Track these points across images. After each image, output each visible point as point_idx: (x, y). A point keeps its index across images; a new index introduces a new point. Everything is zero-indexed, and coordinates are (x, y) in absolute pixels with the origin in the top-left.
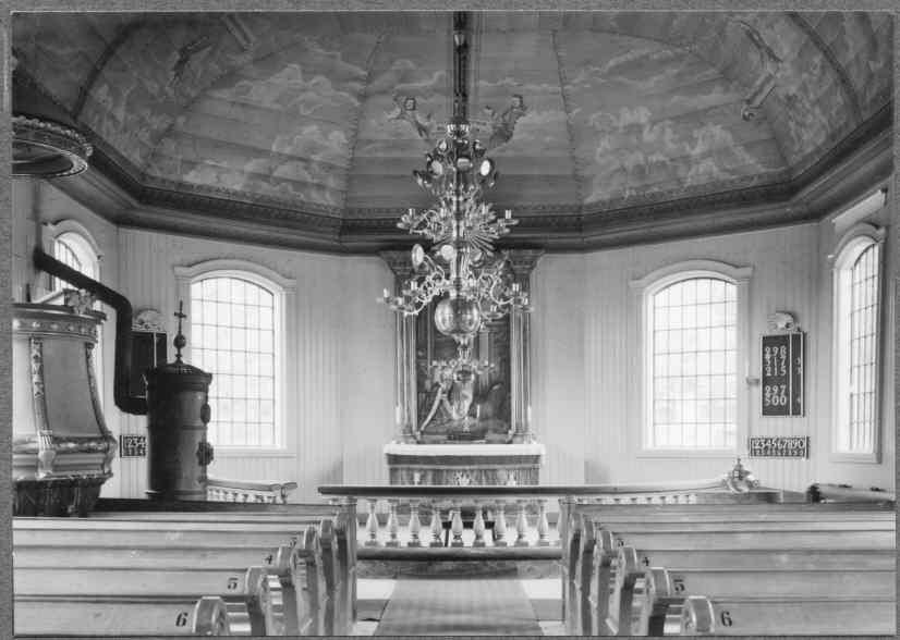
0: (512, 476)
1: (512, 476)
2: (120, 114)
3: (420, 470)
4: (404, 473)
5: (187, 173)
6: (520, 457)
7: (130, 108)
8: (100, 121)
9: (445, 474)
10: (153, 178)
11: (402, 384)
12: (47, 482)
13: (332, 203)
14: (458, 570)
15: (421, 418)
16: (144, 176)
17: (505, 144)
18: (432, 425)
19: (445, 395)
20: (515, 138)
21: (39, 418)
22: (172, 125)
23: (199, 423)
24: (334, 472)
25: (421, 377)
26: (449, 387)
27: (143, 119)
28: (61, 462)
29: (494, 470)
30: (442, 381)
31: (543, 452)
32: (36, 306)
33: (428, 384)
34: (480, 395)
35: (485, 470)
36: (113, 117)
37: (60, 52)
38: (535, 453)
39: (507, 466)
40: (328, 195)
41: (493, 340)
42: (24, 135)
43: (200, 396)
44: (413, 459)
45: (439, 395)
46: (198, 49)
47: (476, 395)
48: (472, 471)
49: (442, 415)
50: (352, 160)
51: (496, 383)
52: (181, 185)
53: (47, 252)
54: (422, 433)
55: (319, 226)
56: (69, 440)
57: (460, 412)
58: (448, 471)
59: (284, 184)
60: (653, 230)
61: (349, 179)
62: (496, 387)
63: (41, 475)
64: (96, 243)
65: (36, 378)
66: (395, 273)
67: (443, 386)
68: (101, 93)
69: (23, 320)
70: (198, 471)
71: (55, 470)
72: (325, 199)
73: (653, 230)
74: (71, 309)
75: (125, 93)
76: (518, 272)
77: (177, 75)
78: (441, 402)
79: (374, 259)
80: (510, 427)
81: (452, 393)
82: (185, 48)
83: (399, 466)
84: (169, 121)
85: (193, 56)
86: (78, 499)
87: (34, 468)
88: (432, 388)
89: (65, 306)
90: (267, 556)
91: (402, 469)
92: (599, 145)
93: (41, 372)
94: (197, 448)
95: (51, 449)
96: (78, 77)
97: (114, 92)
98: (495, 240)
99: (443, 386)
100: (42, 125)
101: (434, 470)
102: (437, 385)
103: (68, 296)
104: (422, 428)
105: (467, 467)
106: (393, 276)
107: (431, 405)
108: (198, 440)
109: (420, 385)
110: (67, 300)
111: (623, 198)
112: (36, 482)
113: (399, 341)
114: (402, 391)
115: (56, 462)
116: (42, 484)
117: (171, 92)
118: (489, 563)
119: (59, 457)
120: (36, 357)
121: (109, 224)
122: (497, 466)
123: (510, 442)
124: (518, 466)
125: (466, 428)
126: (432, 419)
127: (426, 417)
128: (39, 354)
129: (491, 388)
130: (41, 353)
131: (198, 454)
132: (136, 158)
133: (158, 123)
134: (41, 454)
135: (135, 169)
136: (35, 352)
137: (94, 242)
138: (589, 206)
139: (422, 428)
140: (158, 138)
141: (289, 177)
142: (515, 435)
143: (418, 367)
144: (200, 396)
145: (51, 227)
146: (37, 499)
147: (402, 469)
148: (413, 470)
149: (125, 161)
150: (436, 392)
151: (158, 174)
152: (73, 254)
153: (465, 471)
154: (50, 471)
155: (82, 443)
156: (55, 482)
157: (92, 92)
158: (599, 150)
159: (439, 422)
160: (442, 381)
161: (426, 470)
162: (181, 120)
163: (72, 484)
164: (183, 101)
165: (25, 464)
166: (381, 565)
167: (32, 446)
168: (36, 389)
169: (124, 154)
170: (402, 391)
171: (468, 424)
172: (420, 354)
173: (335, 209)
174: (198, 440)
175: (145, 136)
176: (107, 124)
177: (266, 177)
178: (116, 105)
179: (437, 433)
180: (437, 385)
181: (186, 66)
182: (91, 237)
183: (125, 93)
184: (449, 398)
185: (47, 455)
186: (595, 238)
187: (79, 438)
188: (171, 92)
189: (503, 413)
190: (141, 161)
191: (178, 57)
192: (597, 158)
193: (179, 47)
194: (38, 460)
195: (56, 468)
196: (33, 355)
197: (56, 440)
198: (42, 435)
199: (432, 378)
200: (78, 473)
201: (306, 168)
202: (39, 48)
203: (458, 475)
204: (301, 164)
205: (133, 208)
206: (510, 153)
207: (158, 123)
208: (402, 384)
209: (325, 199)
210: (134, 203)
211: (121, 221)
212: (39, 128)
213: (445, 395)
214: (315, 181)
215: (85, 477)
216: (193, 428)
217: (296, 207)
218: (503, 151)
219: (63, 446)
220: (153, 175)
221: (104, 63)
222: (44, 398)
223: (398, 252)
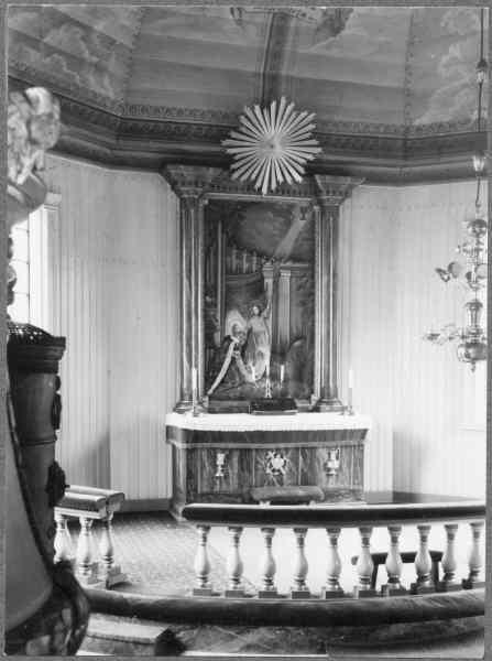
0: (333, 456)
1: (333, 456)
3: (223, 450)
4: (205, 453)
6: (334, 433)
9: (254, 453)
11: (189, 339)
13: (111, 95)
14: (407, 636)
15: (208, 379)
17: (332, 39)
18: (221, 389)
19: (238, 352)
20: (345, 32)
24: (101, 448)
25: (209, 330)
26: (243, 343)
29: (314, 448)
30: (235, 334)
31: (369, 427)
33: (218, 338)
34: (278, 354)
35: (303, 448)
38: (362, 427)
39: (327, 444)
40: (106, 81)
41: (294, 287)
44: (219, 436)
45: (231, 352)
47: (273, 352)
48: (287, 449)
49: (233, 378)
50: (137, 37)
51: (297, 339)
54: (211, 398)
55: (95, 123)
57: (256, 371)
58: (257, 450)
59: (55, 56)
60: (407, 169)
61: (131, 66)
62: (297, 343)
66: (179, 193)
67: (236, 340)
72: (102, 87)
73: (407, 169)
76: (326, 204)
78: (233, 359)
79: (151, 175)
80: (312, 392)
81: (245, 349)
83: (199, 445)
88: (223, 343)
91: (202, 449)
92: (446, 53)
94: (45, 480)
98: (308, 161)
99: (236, 340)
101: (241, 450)
102: (228, 339)
104: (210, 392)
105: (282, 445)
106: (172, 199)
107: (222, 364)
108: (46, 463)
109: (208, 338)
111: (469, 120)
113: (185, 281)
114: (189, 345)
118: (454, 621)
122: (315, 444)
123: (316, 409)
124: (340, 443)
125: (268, 394)
126: (223, 381)
127: (215, 378)
129: (291, 344)
138: (419, 129)
139: (210, 392)
141: (62, 47)
142: (320, 402)
143: (205, 317)
144: (47, 381)
147: (202, 449)
148: (214, 449)
150: (228, 346)
153: (278, 450)
158: (445, 59)
159: (230, 385)
160: (235, 334)
161: (231, 450)
166: (299, 634)
170: (189, 345)
171: (268, 389)
172: (208, 299)
173: (113, 103)
174: (46, 463)
177: (34, 43)
179: (229, 399)
180: (228, 339)
184: (243, 355)
186: (417, 168)
189: (303, 373)
192: (441, 70)
199: (223, 331)
201: (83, 39)
203: (271, 454)
204: (80, 32)
206: (335, 52)
208: (189, 339)
209: (102, 87)
213: (238, 352)
214: (95, 59)
217: (70, 92)
218: (328, 47)
223: (191, 168)
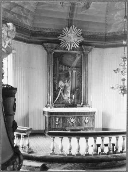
0: (87, 119)
1: (87, 119)
3: (58, 117)
4: (53, 118)
6: (87, 113)
9: (66, 118)
11: (49, 88)
13: (29, 25)
14: (106, 165)
15: (54, 99)
17: (86, 10)
18: (58, 101)
19: (62, 92)
20: (90, 8)
24: (26, 117)
25: (54, 86)
26: (63, 89)
29: (82, 117)
30: (61, 87)
31: (96, 111)
33: (57, 88)
34: (72, 92)
35: (79, 117)
38: (94, 111)
39: (85, 115)
40: (28, 21)
41: (77, 75)
44: (57, 114)
45: (60, 91)
47: (71, 92)
48: (75, 117)
49: (61, 98)
50: (36, 10)
51: (77, 88)
54: (55, 103)
55: (25, 32)
57: (67, 97)
58: (67, 117)
59: (14, 14)
60: (106, 44)
61: (34, 17)
62: (77, 89)
66: (46, 50)
67: (61, 89)
72: (27, 23)
73: (106, 44)
76: (85, 53)
78: (61, 93)
79: (39, 45)
80: (81, 102)
81: (64, 91)
83: (52, 116)
88: (58, 89)
91: (53, 117)
92: (116, 14)
94: (12, 125)
98: (80, 42)
99: (61, 89)
101: (63, 117)
102: (59, 88)
104: (55, 102)
105: (73, 116)
106: (45, 52)
107: (58, 95)
108: (12, 121)
109: (54, 88)
111: (122, 31)
113: (48, 73)
114: (49, 90)
118: (118, 162)
122: (82, 116)
123: (82, 107)
124: (88, 115)
125: (70, 103)
126: (58, 99)
127: (56, 98)
129: (76, 89)
138: (109, 34)
139: (55, 102)
141: (16, 12)
142: (83, 105)
143: (53, 82)
144: (12, 99)
147: (53, 117)
148: (56, 117)
150: (59, 90)
153: (72, 117)
158: (116, 15)
159: (60, 100)
160: (61, 87)
161: (60, 117)
166: (78, 165)
170: (49, 90)
171: (70, 101)
172: (54, 78)
173: (30, 27)
174: (12, 121)
177: (9, 11)
179: (60, 104)
180: (59, 88)
184: (63, 92)
186: (109, 44)
189: (79, 97)
192: (115, 18)
199: (58, 86)
201: (22, 10)
203: (71, 118)
204: (21, 8)
206: (87, 14)
208: (49, 88)
209: (27, 23)
213: (62, 92)
214: (25, 15)
217: (18, 24)
218: (85, 12)
223: (50, 44)
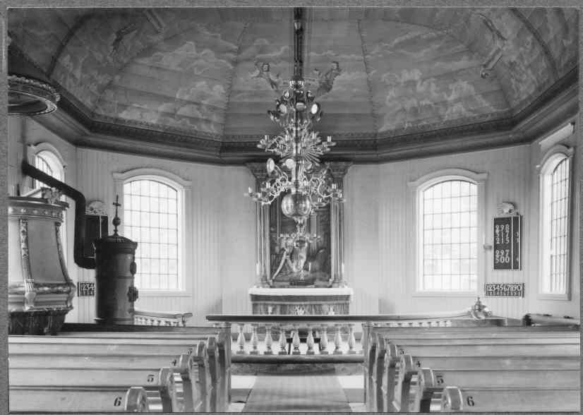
0: (332, 309)
1: (332, 309)
2: (78, 74)
3: (272, 305)
4: (262, 307)
5: (121, 112)
6: (337, 296)
7: (84, 70)
8: (65, 78)
9: (288, 307)
10: (99, 116)
11: (261, 249)
12: (30, 312)
13: (215, 132)
14: (296, 370)
15: (272, 271)
16: (93, 114)
17: (327, 93)
18: (280, 276)
19: (288, 256)
20: (334, 89)
21: (25, 271)
22: (111, 81)
23: (129, 274)
24: (217, 306)
25: (273, 244)
26: (291, 251)
27: (92, 77)
28: (40, 300)
29: (320, 305)
30: (287, 247)
31: (352, 293)
32: (23, 198)
33: (277, 249)
34: (311, 256)
35: (314, 305)
36: (73, 76)
37: (39, 34)
38: (346, 294)
39: (329, 302)
40: (212, 127)
41: (319, 220)
42: (15, 88)
43: (129, 257)
44: (268, 298)
45: (285, 256)
46: (128, 32)
47: (308, 256)
48: (306, 305)
49: (286, 269)
50: (228, 103)
51: (322, 249)
52: (117, 120)
53: (31, 163)
54: (274, 281)
55: (207, 146)
56: (45, 285)
57: (298, 267)
58: (290, 305)
59: (184, 119)
60: (423, 149)
61: (226, 116)
62: (321, 251)
63: (27, 308)
64: (63, 158)
65: (23, 245)
66: (256, 177)
67: (287, 250)
68: (65, 60)
69: (15, 207)
70: (128, 305)
71: (35, 305)
72: (211, 129)
73: (423, 149)
74: (46, 201)
75: (81, 61)
76: (335, 176)
77: (115, 48)
78: (286, 260)
79: (242, 168)
80: (330, 277)
81: (293, 255)
82: (120, 31)
83: (258, 302)
84: (110, 78)
85: (125, 37)
86: (50, 324)
87: (22, 303)
88: (280, 251)
89: (42, 198)
90: (173, 360)
91: (261, 304)
92: (388, 94)
93: (27, 241)
94: (128, 290)
95: (33, 291)
96: (50, 50)
97: (74, 59)
98: (320, 155)
99: (287, 250)
100: (27, 81)
101: (281, 305)
102: (283, 250)
103: (44, 192)
104: (274, 278)
105: (303, 303)
106: (255, 179)
107: (279, 263)
108: (128, 285)
109: (272, 250)
110: (43, 195)
111: (403, 128)
112: (23, 312)
113: (259, 221)
114: (261, 253)
115: (37, 300)
116: (27, 314)
117: (111, 60)
118: (317, 365)
119: (38, 296)
120: (23, 232)
121: (71, 145)
122: (322, 302)
123: (331, 287)
124: (335, 302)
125: (302, 278)
126: (280, 272)
127: (276, 270)
128: (25, 230)
129: (318, 252)
130: (27, 229)
131: (128, 294)
132: (88, 102)
133: (103, 80)
134: (27, 294)
135: (88, 110)
136: (23, 228)
137: (61, 157)
138: (382, 134)
139: (274, 278)
140: (102, 89)
141: (187, 115)
142: (333, 282)
143: (271, 238)
144: (129, 257)
145: (33, 147)
146: (24, 324)
147: (261, 304)
148: (267, 305)
149: (81, 104)
150: (283, 254)
151: (103, 113)
152: (47, 165)
153: (301, 305)
154: (33, 306)
155: (53, 287)
156: (36, 312)
157: (59, 60)
158: (388, 97)
159: (284, 274)
160: (287, 247)
161: (276, 305)
162: (117, 78)
163: (47, 314)
164: (118, 65)
165: (16, 301)
166: (247, 366)
167: (21, 289)
168: (23, 252)
169: (80, 100)
170: (261, 253)
171: (303, 275)
172: (272, 229)
173: (217, 136)
174: (128, 285)
175: (94, 88)
176: (70, 80)
177: (172, 115)
178: (75, 68)
179: (283, 281)
180: (283, 250)
181: (120, 43)
182: (59, 154)
183: (81, 61)
184: (291, 258)
185: (30, 295)
186: (385, 154)
187: (51, 284)
188: (111, 60)
189: (326, 268)
190: (91, 104)
191: (115, 37)
192: (387, 103)
193: (116, 30)
194: (25, 299)
195: (36, 303)
196: (21, 230)
197: (36, 285)
198: (27, 282)
199: (280, 245)
200: (51, 307)
201: (198, 109)
202: (25, 31)
203: (297, 308)
204: (195, 106)
205: (86, 135)
206: (330, 99)
207: (103, 80)
208: (261, 249)
209: (211, 129)
210: (87, 132)
211: (79, 143)
212: (25, 83)
213: (288, 256)
214: (204, 117)
215: (55, 309)
216: (125, 278)
217: (192, 134)
218: (326, 98)
219: (41, 289)
220: (99, 113)
221: (67, 41)
222: (28, 258)
223: (258, 164)
